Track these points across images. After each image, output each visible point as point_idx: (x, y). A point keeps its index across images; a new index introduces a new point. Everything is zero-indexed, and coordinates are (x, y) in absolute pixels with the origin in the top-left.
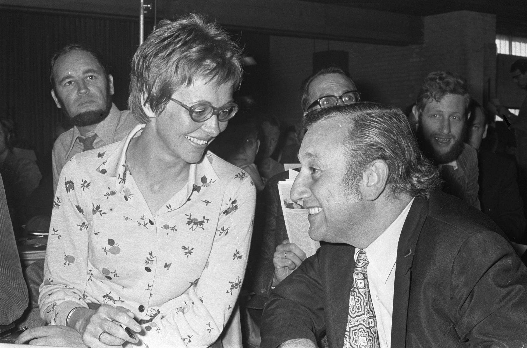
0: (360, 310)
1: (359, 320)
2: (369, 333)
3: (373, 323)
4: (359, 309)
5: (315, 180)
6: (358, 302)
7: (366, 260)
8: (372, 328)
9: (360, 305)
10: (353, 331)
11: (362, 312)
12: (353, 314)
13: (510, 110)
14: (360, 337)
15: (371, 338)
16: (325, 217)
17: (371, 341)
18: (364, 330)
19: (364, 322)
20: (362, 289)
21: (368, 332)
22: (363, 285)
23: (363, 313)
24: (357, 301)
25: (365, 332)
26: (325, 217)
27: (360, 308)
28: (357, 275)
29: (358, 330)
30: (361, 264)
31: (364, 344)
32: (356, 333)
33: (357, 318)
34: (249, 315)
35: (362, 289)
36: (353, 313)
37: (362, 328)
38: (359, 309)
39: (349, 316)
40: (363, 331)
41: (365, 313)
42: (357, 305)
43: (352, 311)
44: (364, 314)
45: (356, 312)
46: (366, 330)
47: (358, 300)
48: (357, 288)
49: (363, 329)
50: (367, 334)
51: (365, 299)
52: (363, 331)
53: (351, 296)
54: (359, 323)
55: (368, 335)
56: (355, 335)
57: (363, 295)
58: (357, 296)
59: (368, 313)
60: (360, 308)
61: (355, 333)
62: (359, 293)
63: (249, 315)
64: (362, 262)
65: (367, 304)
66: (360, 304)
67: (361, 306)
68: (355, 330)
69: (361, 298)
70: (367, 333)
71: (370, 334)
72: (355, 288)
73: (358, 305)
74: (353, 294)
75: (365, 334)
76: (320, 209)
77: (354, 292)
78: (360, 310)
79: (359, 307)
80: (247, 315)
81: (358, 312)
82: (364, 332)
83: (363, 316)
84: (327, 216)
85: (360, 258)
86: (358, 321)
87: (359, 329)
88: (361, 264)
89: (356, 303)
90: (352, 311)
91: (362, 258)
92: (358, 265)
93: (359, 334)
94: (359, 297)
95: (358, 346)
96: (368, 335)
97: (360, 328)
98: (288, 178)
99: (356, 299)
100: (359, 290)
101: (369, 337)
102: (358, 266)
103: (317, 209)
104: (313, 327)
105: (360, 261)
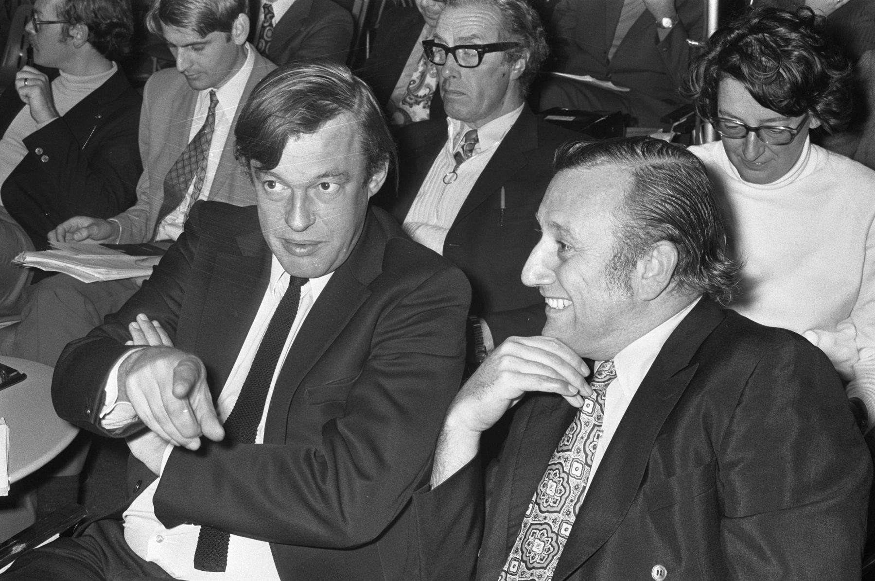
0: (556, 505)
1: (548, 518)
4: (555, 503)
5: (564, 261)
6: (560, 493)
7: (612, 372)
8: (561, 536)
9: (559, 499)
10: (533, 529)
11: (558, 509)
12: (544, 507)
14: (551, 481)
15: (552, 549)
16: (575, 317)
17: (561, 494)
18: (547, 534)
19: (553, 522)
20: (574, 477)
21: (552, 538)
22: (578, 473)
23: (570, 448)
24: (559, 491)
25: (548, 537)
26: (575, 317)
27: (558, 503)
28: (586, 424)
29: (540, 531)
30: (603, 376)
31: (537, 551)
32: (536, 533)
33: (547, 514)
35: (585, 414)
37: (546, 530)
38: (555, 503)
40: (558, 474)
41: (573, 449)
44: (559, 512)
45: (549, 505)
46: (550, 535)
47: (561, 490)
48: (568, 475)
50: (560, 481)
51: (582, 429)
54: (546, 521)
55: (561, 482)
56: (532, 536)
57: (572, 487)
58: (562, 485)
59: (578, 453)
60: (558, 503)
61: (534, 533)
62: (568, 482)
64: (605, 374)
65: (572, 501)
66: (561, 497)
67: (561, 499)
68: (536, 529)
69: (565, 492)
70: (550, 539)
71: (554, 543)
72: (564, 472)
73: (557, 498)
74: (556, 481)
75: (559, 479)
76: (567, 303)
78: (556, 505)
79: (557, 500)
81: (552, 506)
82: (546, 535)
83: (556, 514)
84: (578, 315)
85: (602, 369)
86: (545, 518)
87: (542, 530)
88: (603, 376)
89: (544, 552)
90: (544, 502)
91: (607, 368)
92: (597, 377)
93: (539, 536)
94: (552, 546)
96: (561, 482)
97: (543, 529)
98: (620, 112)
99: (559, 488)
100: (570, 477)
101: (550, 546)
102: (597, 380)
103: (561, 301)
105: (603, 373)
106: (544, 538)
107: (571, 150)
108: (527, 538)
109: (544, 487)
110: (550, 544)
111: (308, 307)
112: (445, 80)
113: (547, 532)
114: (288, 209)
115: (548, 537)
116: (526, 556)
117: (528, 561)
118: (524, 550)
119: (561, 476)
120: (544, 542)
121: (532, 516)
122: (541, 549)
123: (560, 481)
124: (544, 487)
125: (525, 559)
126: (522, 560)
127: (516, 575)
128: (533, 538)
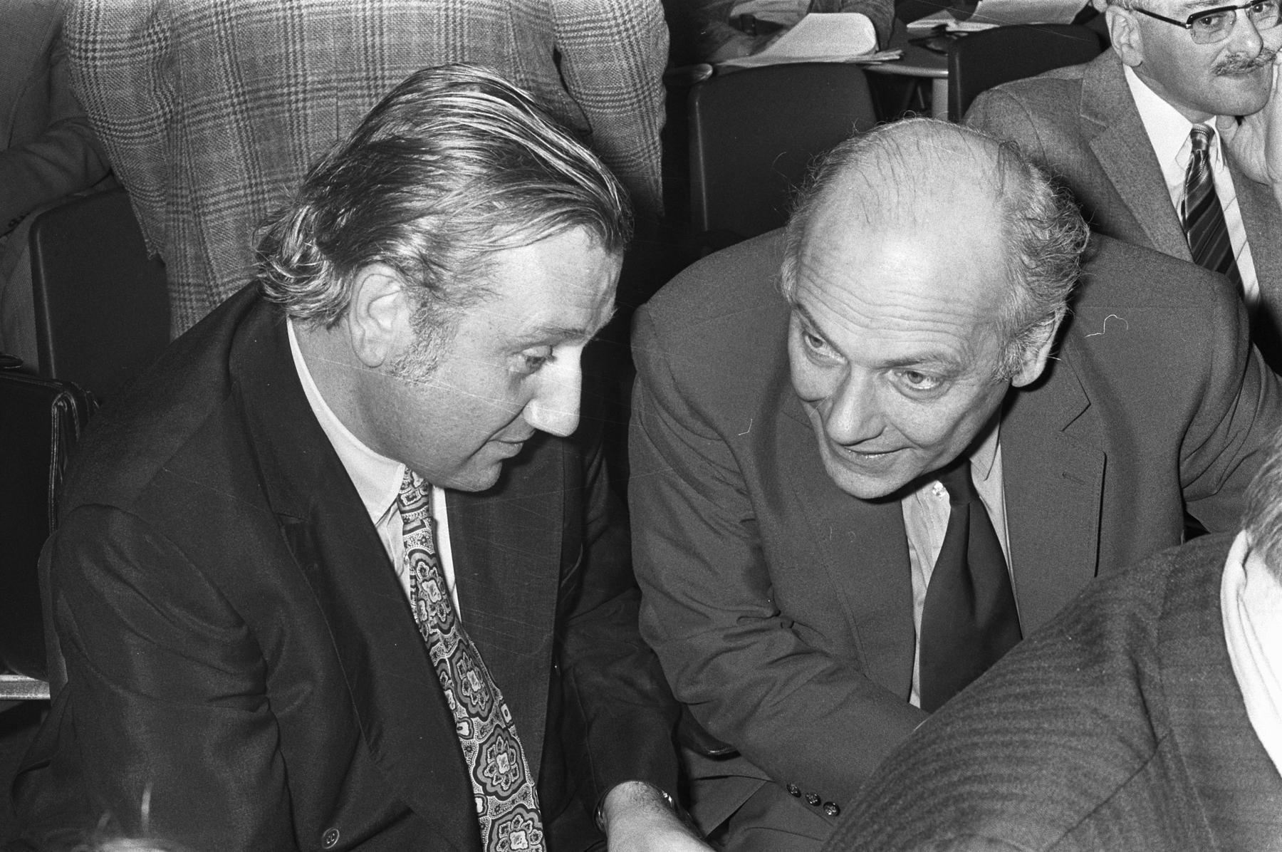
2: (533, 822)
3: (503, 711)
13: (909, 26)
18: (427, 564)
19: (422, 543)
21: (532, 819)
29: (511, 821)
34: (921, 582)
36: (420, 563)
39: (461, 740)
40: (425, 566)
42: (531, 847)
46: (527, 816)
49: (424, 561)
50: (529, 825)
52: (425, 566)
54: (510, 799)
63: (921, 582)
70: (530, 822)
75: (432, 571)
80: (928, 602)
82: (427, 568)
86: (513, 802)
95: (531, 828)
104: (475, 124)
106: (522, 825)
107: (193, 566)
108: (459, 682)
109: (466, 689)
110: (534, 828)
111: (1236, 656)
112: (1155, 752)
113: (424, 561)
114: (1135, 747)
115: (525, 821)
116: (474, 706)
117: (480, 710)
118: (466, 701)
119: (526, 818)
120: (522, 830)
121: (476, 734)
122: (524, 840)
123: (529, 825)
124: (466, 689)
125: (473, 711)
126: (471, 715)
127: (486, 815)
128: (505, 835)
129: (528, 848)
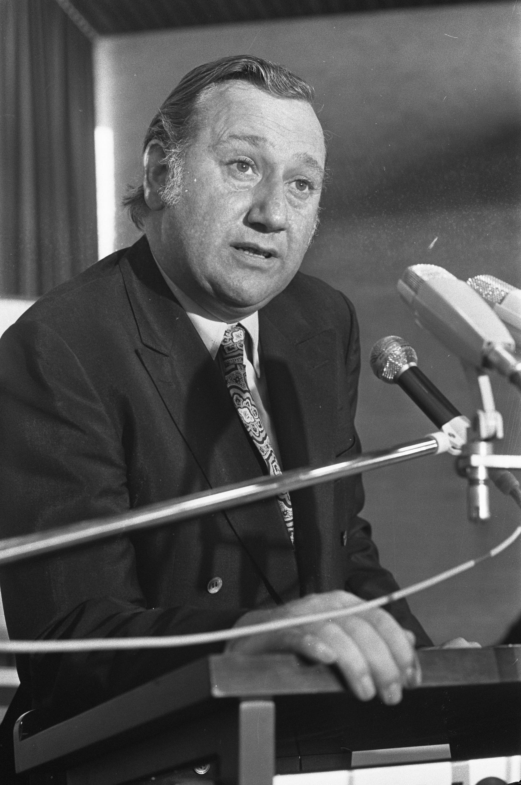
43: (254, 432)
53: (240, 410)
58: (252, 405)
75: (245, 402)
77: (244, 400)
123: (248, 403)
129: (255, 421)
